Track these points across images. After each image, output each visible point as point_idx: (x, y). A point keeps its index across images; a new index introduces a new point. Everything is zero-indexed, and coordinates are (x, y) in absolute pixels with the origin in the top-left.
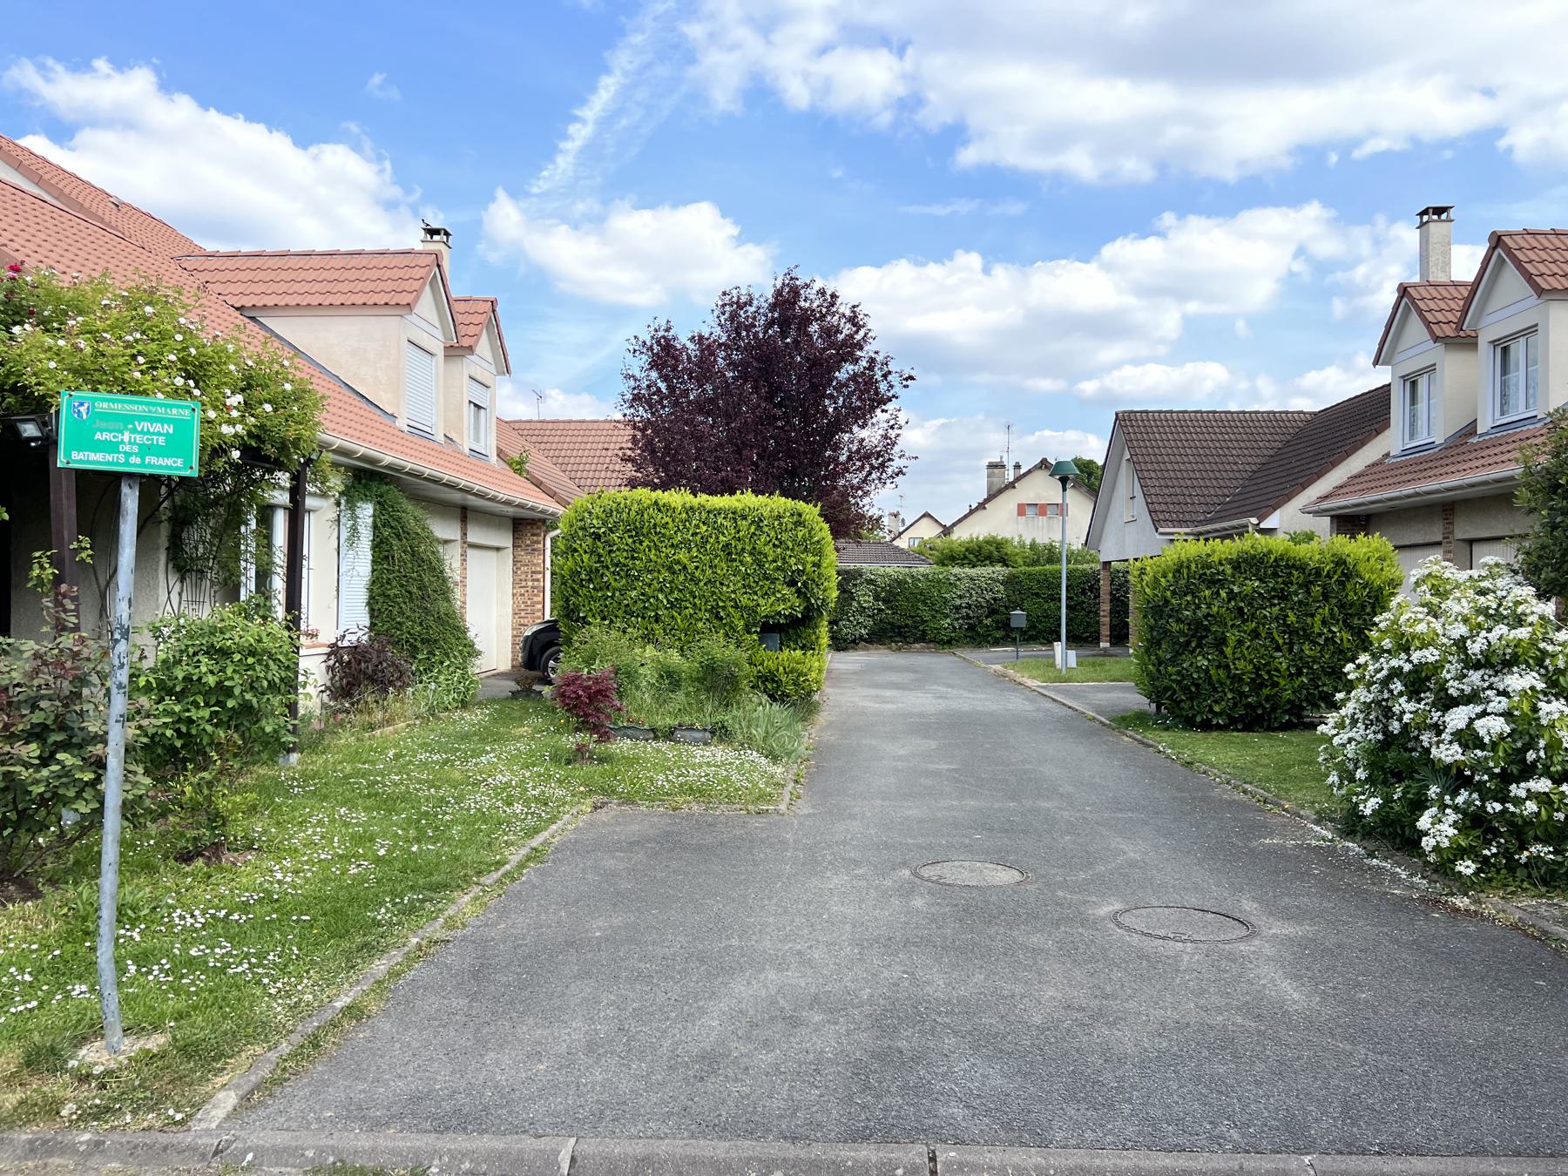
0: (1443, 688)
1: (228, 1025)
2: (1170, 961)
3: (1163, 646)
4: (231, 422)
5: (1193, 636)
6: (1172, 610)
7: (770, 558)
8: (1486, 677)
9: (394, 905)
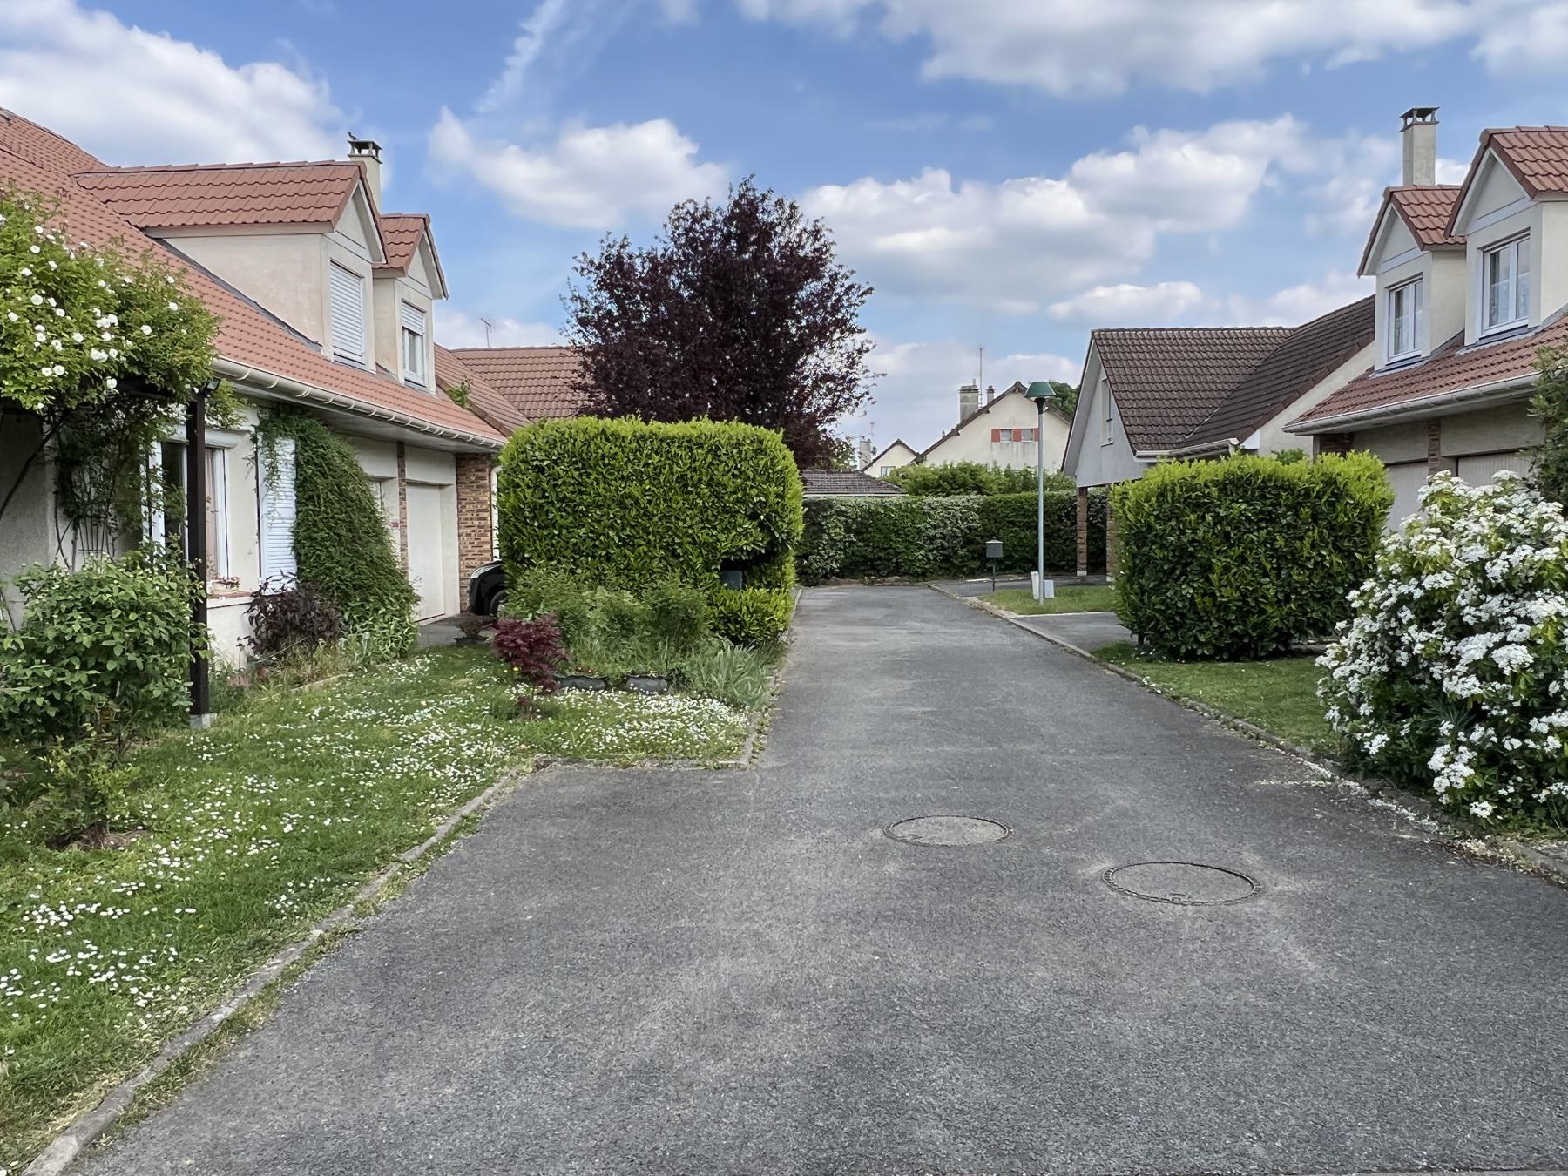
0: (1457, 615)
1: (81, 1051)
2: (1170, 928)
3: (1147, 574)
4: (102, 346)
5: (1178, 563)
6: (1156, 536)
7: (729, 490)
8: (1506, 603)
9: (298, 889)
